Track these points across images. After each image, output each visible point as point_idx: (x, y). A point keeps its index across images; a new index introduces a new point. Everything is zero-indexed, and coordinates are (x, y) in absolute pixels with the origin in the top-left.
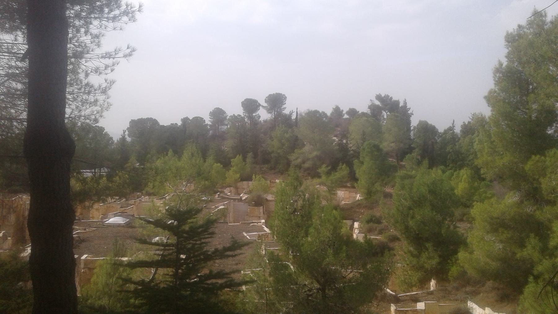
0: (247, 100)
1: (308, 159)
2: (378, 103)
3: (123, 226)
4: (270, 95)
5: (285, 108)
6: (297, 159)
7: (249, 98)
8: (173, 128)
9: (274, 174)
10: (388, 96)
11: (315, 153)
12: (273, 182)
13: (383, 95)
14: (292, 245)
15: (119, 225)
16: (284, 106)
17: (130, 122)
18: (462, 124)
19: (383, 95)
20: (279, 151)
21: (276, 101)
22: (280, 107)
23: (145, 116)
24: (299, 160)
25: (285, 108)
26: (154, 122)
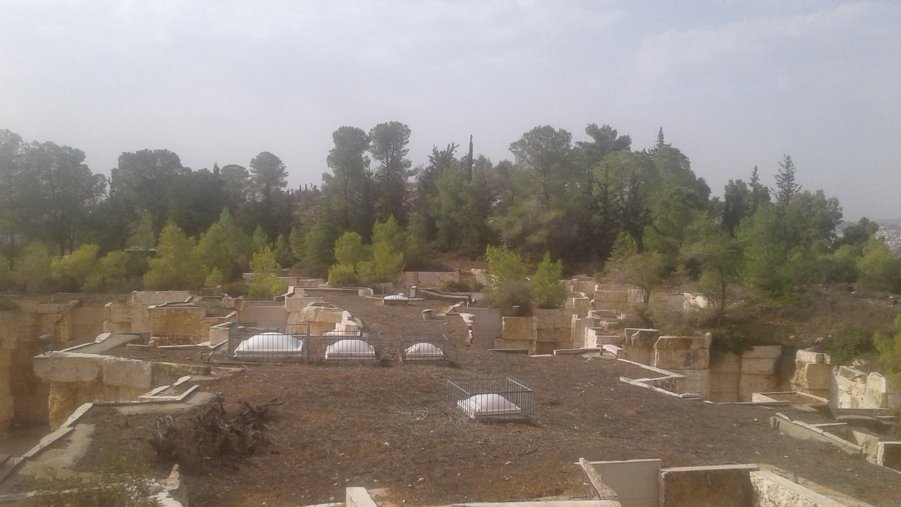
0: (342, 129)
1: (540, 226)
2: (591, 140)
3: (301, 361)
4: (379, 126)
5: (406, 151)
6: (510, 225)
7: (348, 124)
8: (204, 173)
9: (457, 258)
10: (609, 128)
12: (465, 274)
13: (600, 127)
14: (243, 419)
15: (287, 359)
16: (405, 147)
17: (120, 158)
18: (727, 183)
19: (600, 127)
20: (452, 215)
21: (392, 137)
22: (397, 149)
23: (153, 144)
24: (518, 229)
25: (406, 151)
26: (172, 160)
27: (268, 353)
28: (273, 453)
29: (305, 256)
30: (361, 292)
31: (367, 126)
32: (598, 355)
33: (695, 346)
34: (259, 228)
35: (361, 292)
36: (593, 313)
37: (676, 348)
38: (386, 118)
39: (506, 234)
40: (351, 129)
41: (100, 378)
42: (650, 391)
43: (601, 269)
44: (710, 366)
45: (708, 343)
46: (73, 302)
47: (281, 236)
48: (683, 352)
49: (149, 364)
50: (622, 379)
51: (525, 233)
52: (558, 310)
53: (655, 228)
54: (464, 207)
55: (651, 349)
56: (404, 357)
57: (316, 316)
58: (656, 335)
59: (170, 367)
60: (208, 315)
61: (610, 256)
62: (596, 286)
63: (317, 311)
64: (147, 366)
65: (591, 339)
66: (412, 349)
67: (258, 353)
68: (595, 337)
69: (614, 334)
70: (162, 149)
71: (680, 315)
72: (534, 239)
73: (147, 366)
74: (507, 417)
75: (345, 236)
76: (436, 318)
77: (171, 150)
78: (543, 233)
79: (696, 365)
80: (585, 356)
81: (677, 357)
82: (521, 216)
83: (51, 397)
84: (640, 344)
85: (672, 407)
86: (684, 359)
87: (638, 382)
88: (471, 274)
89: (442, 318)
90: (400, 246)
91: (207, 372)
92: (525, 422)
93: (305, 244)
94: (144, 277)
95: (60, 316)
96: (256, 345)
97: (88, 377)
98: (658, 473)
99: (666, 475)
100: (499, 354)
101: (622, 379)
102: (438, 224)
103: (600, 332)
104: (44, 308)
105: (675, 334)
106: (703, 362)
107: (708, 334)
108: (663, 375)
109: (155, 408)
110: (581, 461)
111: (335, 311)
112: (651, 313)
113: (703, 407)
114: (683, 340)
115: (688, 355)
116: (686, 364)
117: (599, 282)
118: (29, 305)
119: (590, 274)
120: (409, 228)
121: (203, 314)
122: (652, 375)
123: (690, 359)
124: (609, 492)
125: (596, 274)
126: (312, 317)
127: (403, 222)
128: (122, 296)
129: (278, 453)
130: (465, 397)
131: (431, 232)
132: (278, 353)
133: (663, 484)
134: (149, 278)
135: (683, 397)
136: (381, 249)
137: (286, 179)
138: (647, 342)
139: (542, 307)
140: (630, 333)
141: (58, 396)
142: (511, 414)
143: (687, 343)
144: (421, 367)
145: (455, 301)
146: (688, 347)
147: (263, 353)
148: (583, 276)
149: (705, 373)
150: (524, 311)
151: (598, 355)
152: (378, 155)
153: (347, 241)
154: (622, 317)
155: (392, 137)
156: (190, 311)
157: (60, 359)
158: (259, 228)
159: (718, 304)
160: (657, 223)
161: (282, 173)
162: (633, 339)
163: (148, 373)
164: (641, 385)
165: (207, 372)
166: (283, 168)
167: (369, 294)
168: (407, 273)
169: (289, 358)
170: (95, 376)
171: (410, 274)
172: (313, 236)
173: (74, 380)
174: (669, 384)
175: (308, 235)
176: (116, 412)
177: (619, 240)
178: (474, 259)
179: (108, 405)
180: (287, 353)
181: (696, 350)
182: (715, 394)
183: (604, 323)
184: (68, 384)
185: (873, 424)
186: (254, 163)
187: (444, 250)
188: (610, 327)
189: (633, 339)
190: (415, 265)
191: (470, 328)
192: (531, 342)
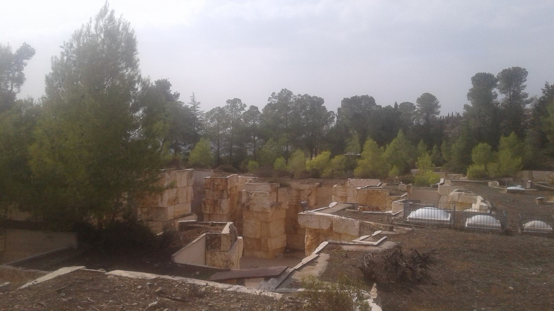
0: (477, 75)
5: (524, 87)
7: (482, 71)
16: (524, 84)
17: (342, 101)
25: (524, 87)
26: (370, 101)
28: (433, 284)
29: (450, 159)
30: (490, 183)
31: (495, 71)
34: (422, 141)
35: (490, 183)
38: (509, 65)
40: (485, 74)
47: (435, 146)
56: (522, 229)
57: (459, 198)
59: (370, 224)
60: (391, 194)
64: (357, 222)
66: (528, 225)
67: (422, 220)
70: (365, 95)
73: (357, 222)
77: (370, 95)
91: (391, 229)
93: (452, 151)
94: (355, 170)
95: (310, 191)
96: (482, 220)
97: (325, 226)
104: (303, 187)
109: (362, 248)
111: (472, 195)
118: (295, 184)
121: (388, 194)
126: (456, 199)
127: (521, 136)
128: (342, 182)
129: (436, 285)
132: (434, 220)
134: (358, 171)
136: (505, 155)
137: (439, 109)
144: (536, 237)
147: (425, 220)
152: (503, 91)
153: (480, 150)
155: (514, 77)
156: (380, 192)
157: (311, 215)
158: (422, 141)
161: (436, 106)
163: (357, 227)
166: (438, 103)
167: (496, 185)
168: (524, 171)
169: (442, 224)
170: (329, 226)
171: (526, 173)
172: (457, 146)
175: (453, 146)
179: (336, 244)
180: (441, 221)
184: (315, 230)
185: (14, 75)
186: (419, 100)
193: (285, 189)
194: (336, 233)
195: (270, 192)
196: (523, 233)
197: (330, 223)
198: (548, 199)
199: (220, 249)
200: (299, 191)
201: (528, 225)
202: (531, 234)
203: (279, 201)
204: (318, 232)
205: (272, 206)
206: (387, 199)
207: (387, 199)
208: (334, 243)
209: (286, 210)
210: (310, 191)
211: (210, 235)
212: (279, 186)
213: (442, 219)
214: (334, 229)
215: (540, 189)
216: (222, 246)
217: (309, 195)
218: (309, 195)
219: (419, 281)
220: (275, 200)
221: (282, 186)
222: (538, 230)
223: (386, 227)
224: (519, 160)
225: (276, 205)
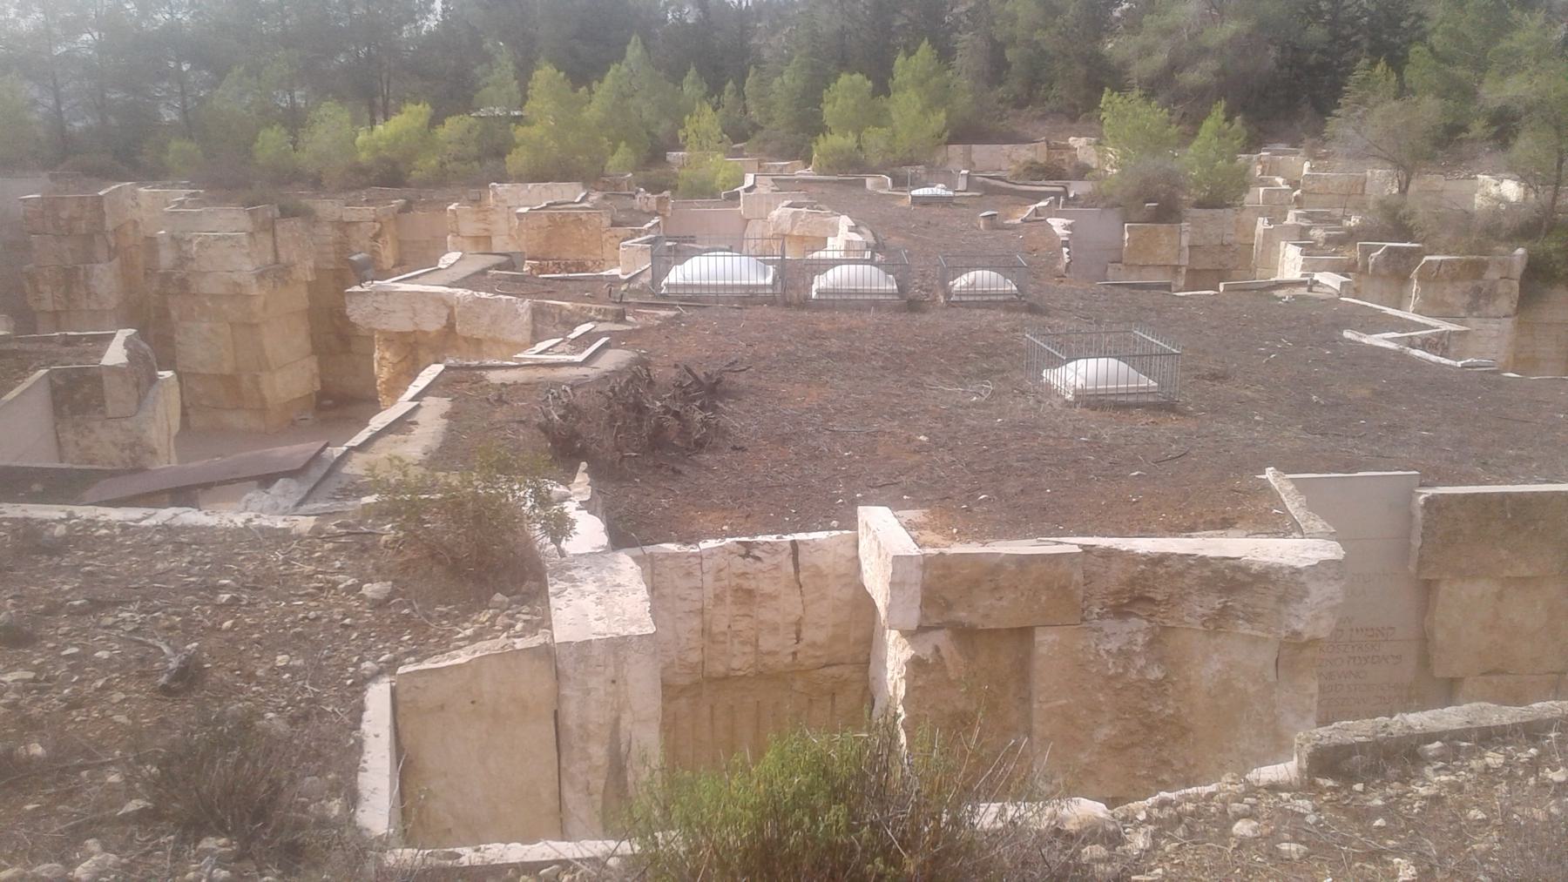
1: (1204, 52)
6: (1147, 52)
9: (1043, 118)
11: (1232, 27)
12: (1057, 147)
20: (1036, 38)
24: (1160, 59)
27: (716, 287)
28: (734, 448)
29: (770, 119)
30: (870, 182)
32: (1303, 291)
33: (1492, 274)
34: (692, 72)
35: (870, 182)
36: (1297, 216)
37: (1453, 279)
39: (1141, 69)
41: (450, 326)
42: (1399, 354)
43: (1317, 133)
44: (1517, 311)
45: (1518, 268)
46: (398, 202)
48: (1469, 284)
49: (527, 303)
50: (1347, 334)
51: (1173, 67)
52: (1229, 211)
53: (1432, 50)
54: (1059, 21)
55: (1404, 280)
56: (948, 295)
57: (793, 225)
58: (1419, 253)
60: (615, 224)
61: (1338, 106)
62: (1307, 165)
63: (795, 216)
65: (1290, 263)
66: (961, 282)
67: (700, 286)
68: (1300, 260)
69: (1335, 253)
71: (1468, 215)
72: (1192, 77)
74: (1131, 399)
75: (840, 81)
76: (1005, 228)
78: (1211, 65)
79: (1491, 310)
80: (1279, 293)
81: (1456, 295)
82: (1167, 33)
83: (376, 355)
84: (1384, 271)
85: (1440, 382)
86: (1467, 299)
87: (1381, 340)
88: (1068, 148)
89: (1014, 227)
90: (939, 98)
92: (1165, 406)
93: (772, 97)
95: (378, 226)
98: (1410, 496)
99: (1427, 500)
100: (1117, 290)
101: (1347, 334)
102: (1010, 54)
103: (1309, 249)
104: (351, 214)
105: (1456, 253)
106: (1505, 304)
107: (1520, 251)
108: (1427, 327)
110: (1270, 474)
111: (826, 216)
112: (1412, 214)
113: (1501, 384)
114: (1471, 262)
115: (1477, 292)
116: (1472, 308)
117: (1313, 156)
118: (329, 208)
119: (1295, 143)
120: (958, 62)
121: (607, 222)
122: (1406, 326)
123: (1480, 298)
124: (1319, 525)
125: (1308, 141)
126: (786, 227)
127: (945, 54)
129: (742, 449)
130: (1056, 363)
131: (997, 69)
132: (733, 287)
133: (1419, 515)
134: (516, 160)
135: (1464, 366)
136: (906, 104)
138: (1398, 270)
139: (1200, 205)
140: (1367, 252)
141: (387, 355)
142: (1148, 392)
143: (1477, 269)
145: (1038, 196)
146: (1479, 276)
147: (709, 287)
148: (1281, 147)
149: (1508, 324)
150: (1167, 212)
151: (1303, 291)
154: (1354, 221)
156: (584, 217)
157: (386, 294)
159: (1546, 196)
160: (1435, 39)
162: (1371, 261)
163: (526, 318)
164: (1382, 344)
165: (620, 317)
168: (951, 147)
169: (752, 296)
170: (444, 322)
171: (956, 150)
172: (787, 82)
173: (409, 327)
174: (1437, 343)
176: (482, 378)
177: (1359, 75)
178: (1073, 119)
179: (468, 368)
180: (749, 286)
181: (1494, 282)
182: (1522, 362)
183: (1318, 233)
187: (1020, 104)
188: (1328, 241)
189: (1371, 261)
190: (966, 133)
191: (1066, 244)
192: (1176, 269)
193: (297, 223)
194: (465, 339)
195: (251, 234)
196: (950, 304)
197: (445, 312)
198: (1007, 216)
199: (102, 412)
200: (343, 226)
201: (961, 282)
202: (968, 305)
203: (283, 258)
204: (412, 340)
205: (261, 276)
206: (605, 236)
207: (605, 236)
208: (461, 368)
209: (309, 284)
210: (378, 226)
211: (62, 373)
212: (277, 213)
213: (753, 282)
214: (458, 328)
215: (989, 190)
216: (108, 403)
217: (376, 237)
218: (376, 237)
219: (700, 445)
220: (270, 258)
221: (287, 212)
222: (984, 294)
223: (606, 312)
224: (939, 118)
225: (277, 272)
